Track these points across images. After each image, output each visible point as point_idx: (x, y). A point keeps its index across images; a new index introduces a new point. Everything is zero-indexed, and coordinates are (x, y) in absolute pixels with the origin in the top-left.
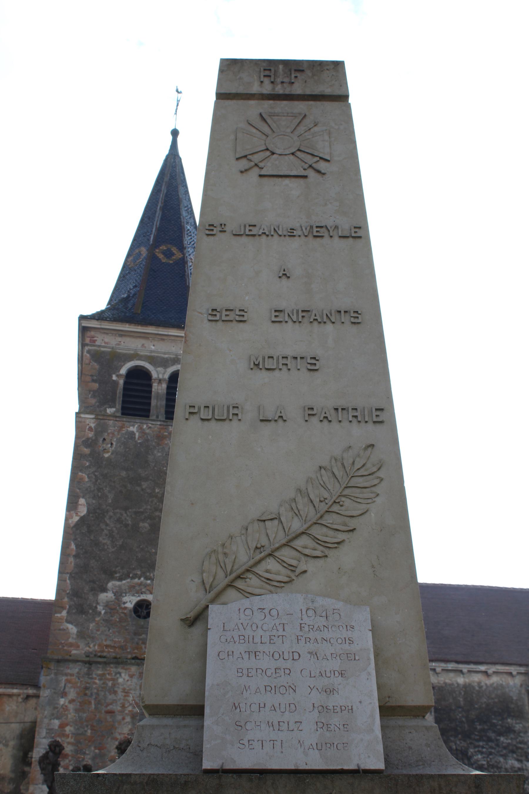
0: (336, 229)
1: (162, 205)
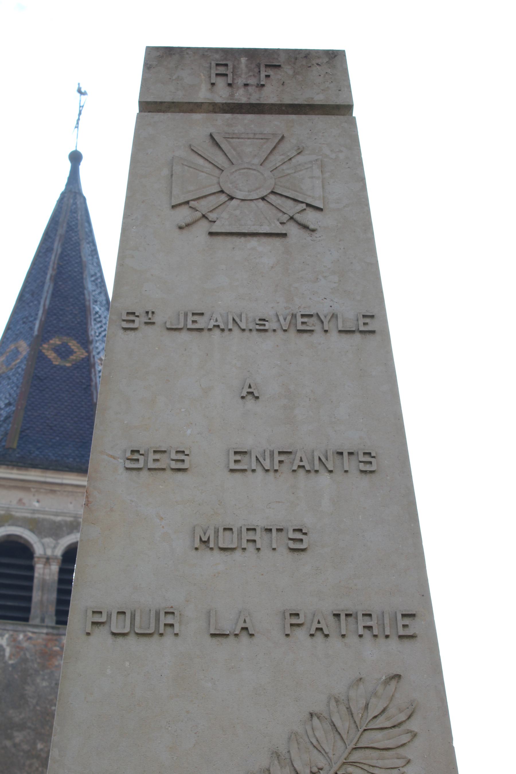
0: (334, 320)
1: (54, 273)
